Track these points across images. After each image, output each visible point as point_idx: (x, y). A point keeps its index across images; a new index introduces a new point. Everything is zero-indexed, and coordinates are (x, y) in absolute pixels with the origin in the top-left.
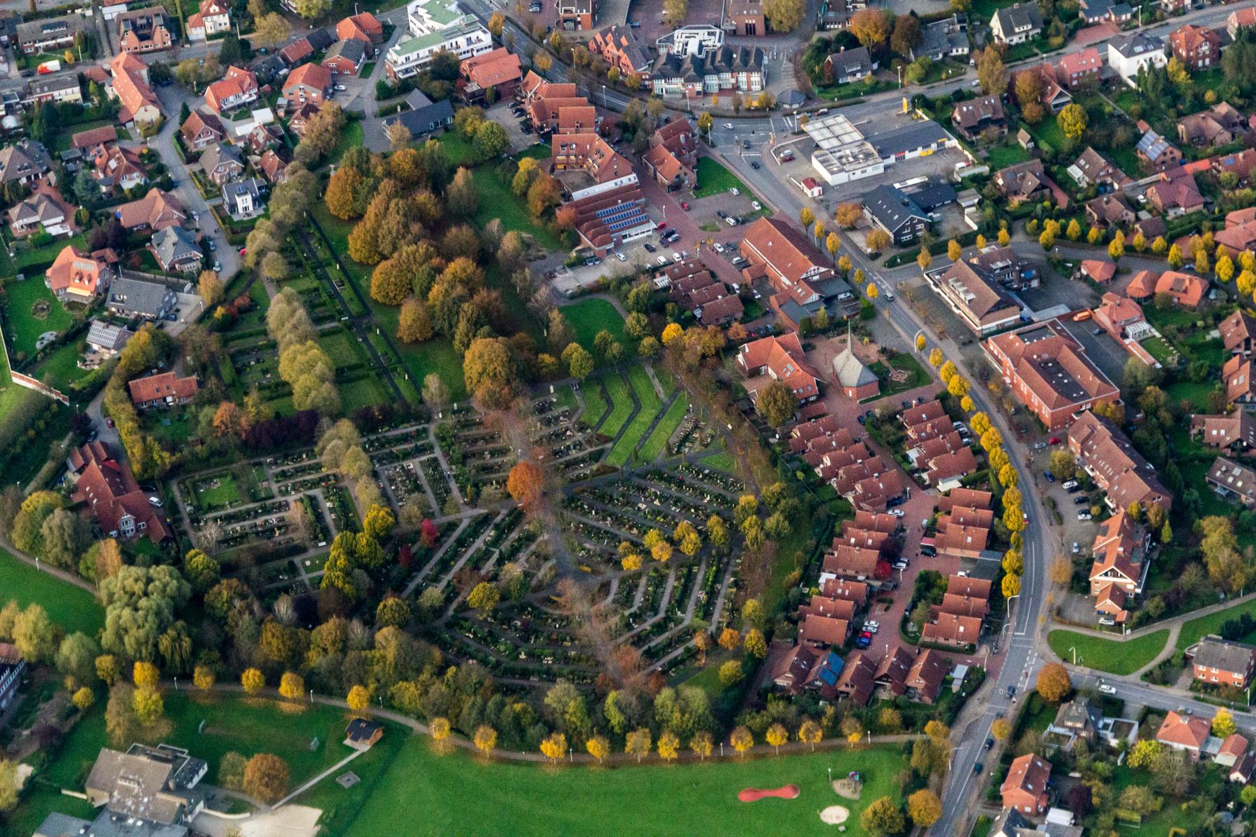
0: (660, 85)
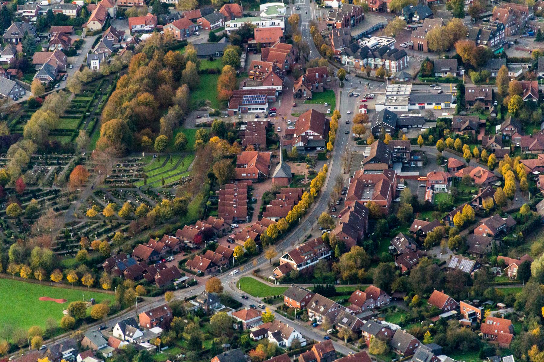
0: (345, 59)
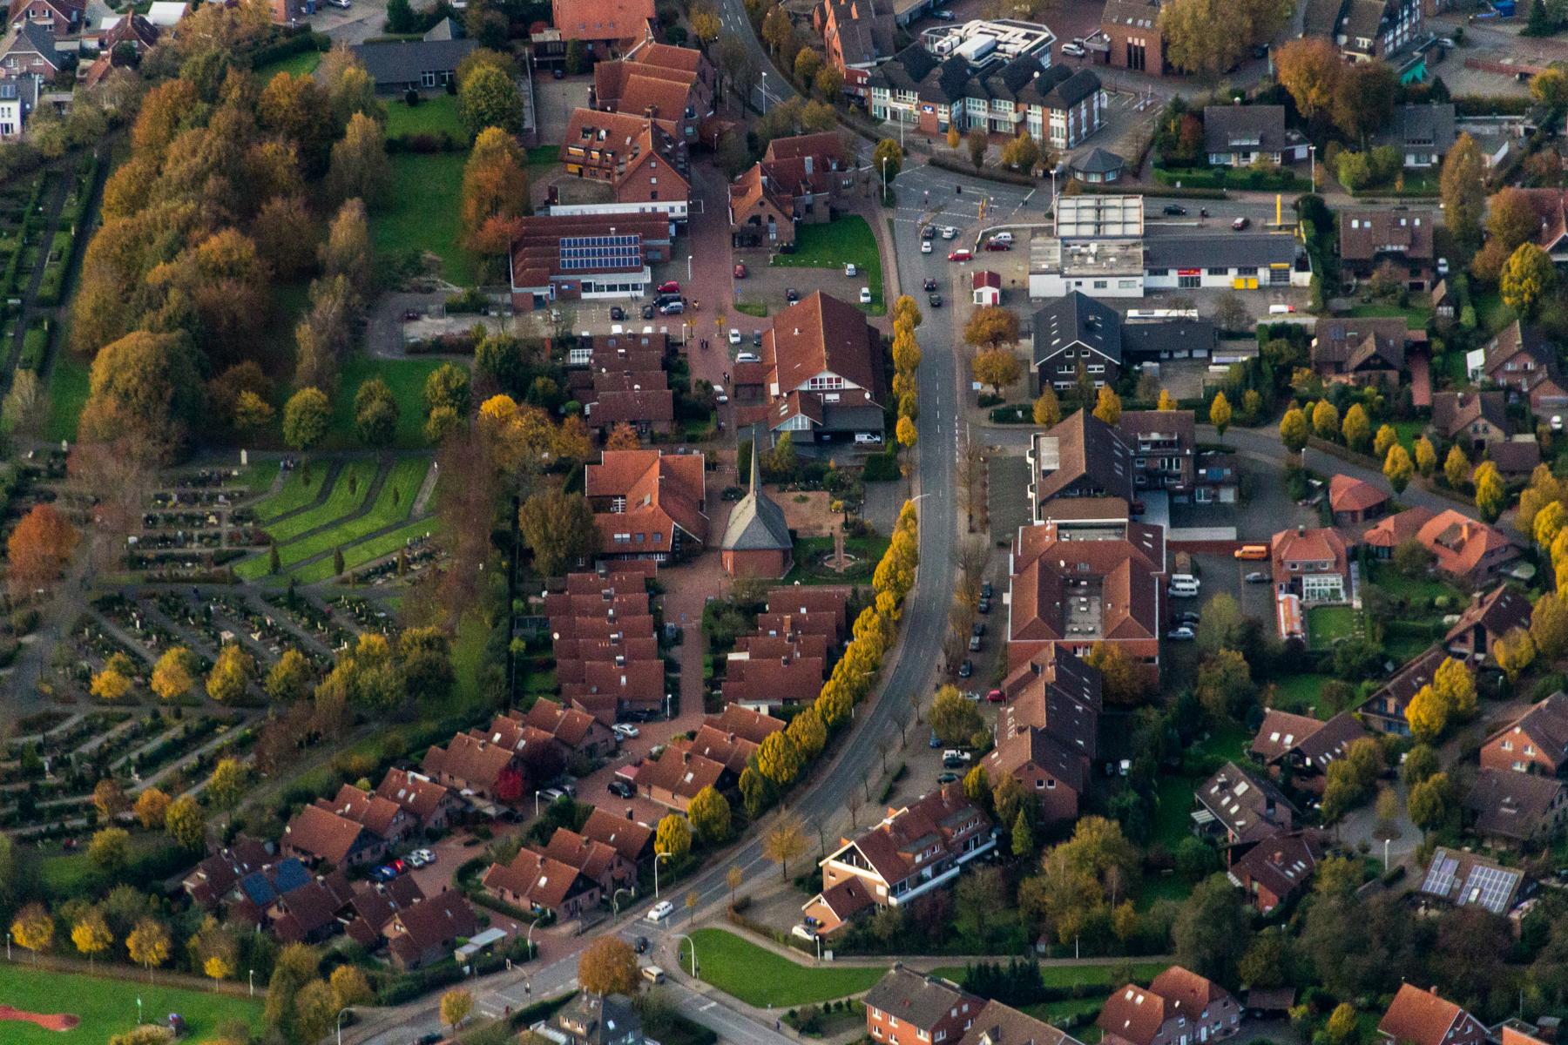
0: (882, 99)
